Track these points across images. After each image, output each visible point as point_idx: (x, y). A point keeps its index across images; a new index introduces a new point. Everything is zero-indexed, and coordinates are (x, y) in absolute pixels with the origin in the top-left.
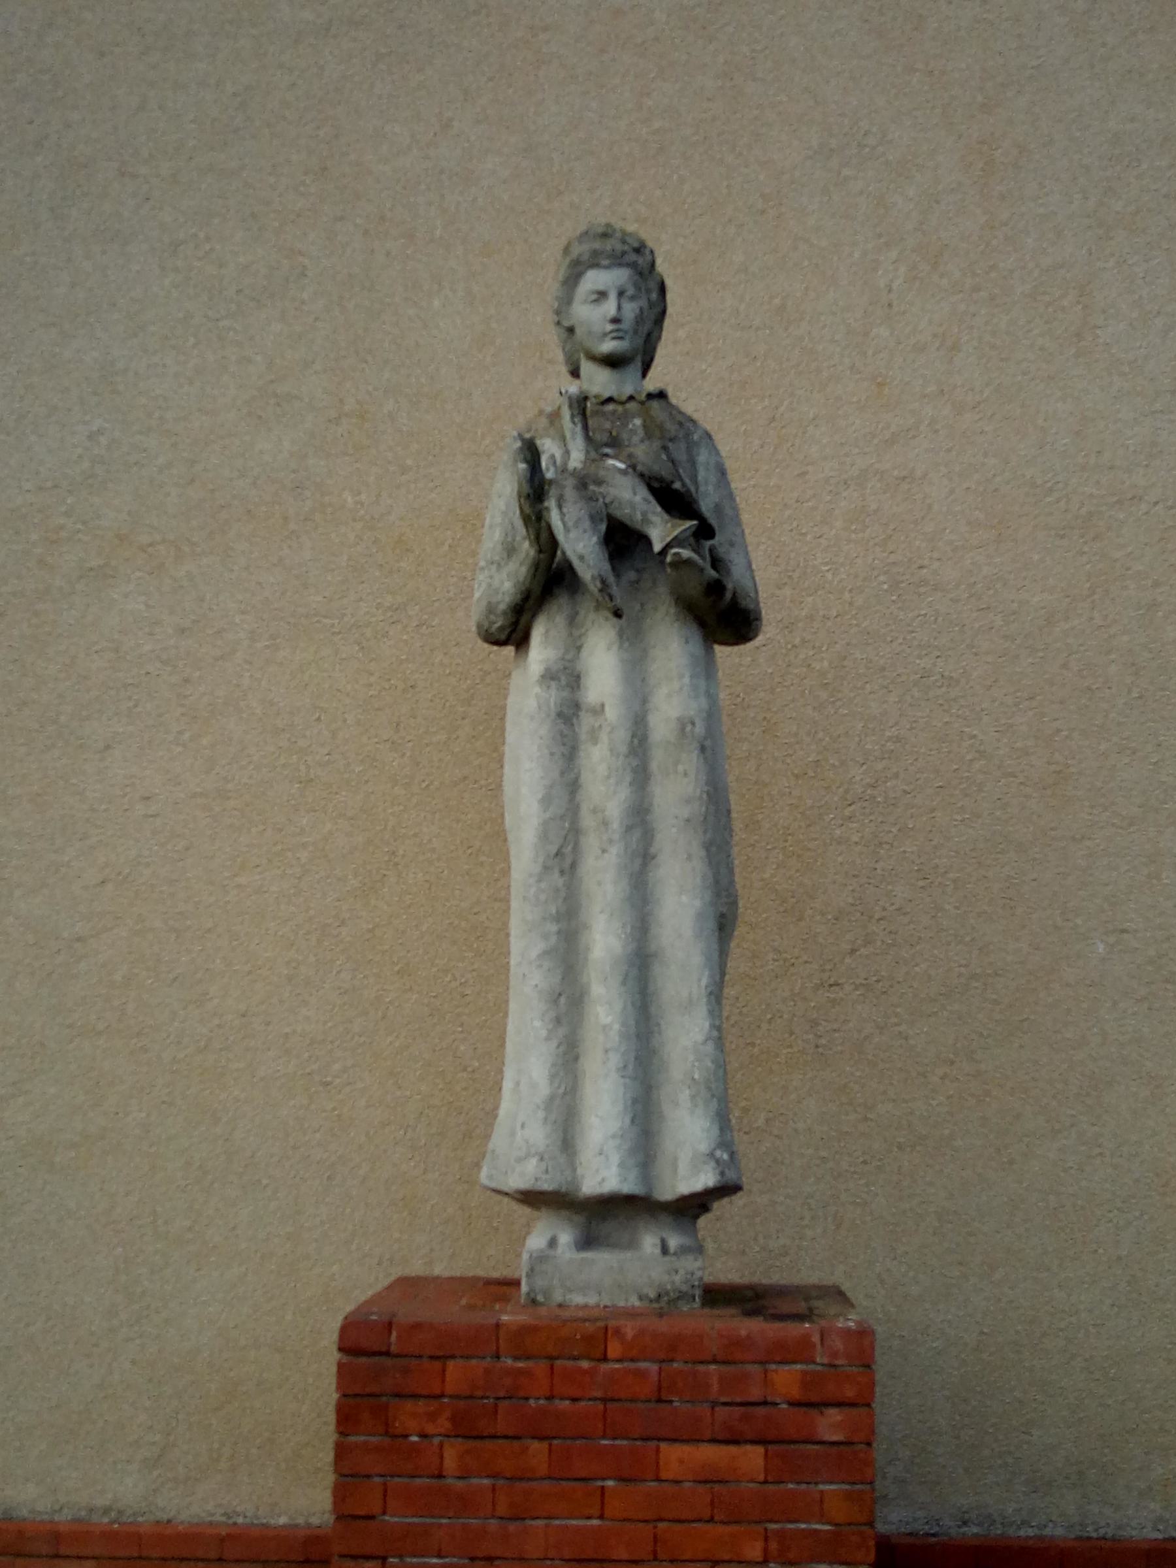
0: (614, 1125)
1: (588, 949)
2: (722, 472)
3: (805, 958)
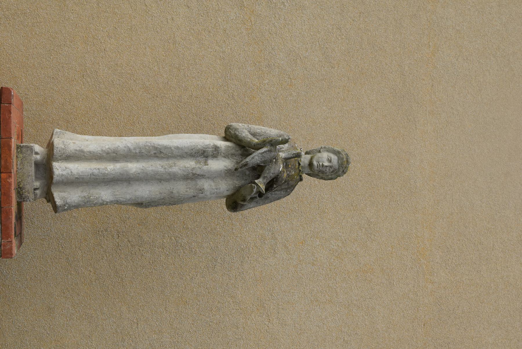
0: (75, 172)
1: (131, 162)
2: (279, 199)
3: (127, 227)
